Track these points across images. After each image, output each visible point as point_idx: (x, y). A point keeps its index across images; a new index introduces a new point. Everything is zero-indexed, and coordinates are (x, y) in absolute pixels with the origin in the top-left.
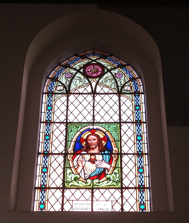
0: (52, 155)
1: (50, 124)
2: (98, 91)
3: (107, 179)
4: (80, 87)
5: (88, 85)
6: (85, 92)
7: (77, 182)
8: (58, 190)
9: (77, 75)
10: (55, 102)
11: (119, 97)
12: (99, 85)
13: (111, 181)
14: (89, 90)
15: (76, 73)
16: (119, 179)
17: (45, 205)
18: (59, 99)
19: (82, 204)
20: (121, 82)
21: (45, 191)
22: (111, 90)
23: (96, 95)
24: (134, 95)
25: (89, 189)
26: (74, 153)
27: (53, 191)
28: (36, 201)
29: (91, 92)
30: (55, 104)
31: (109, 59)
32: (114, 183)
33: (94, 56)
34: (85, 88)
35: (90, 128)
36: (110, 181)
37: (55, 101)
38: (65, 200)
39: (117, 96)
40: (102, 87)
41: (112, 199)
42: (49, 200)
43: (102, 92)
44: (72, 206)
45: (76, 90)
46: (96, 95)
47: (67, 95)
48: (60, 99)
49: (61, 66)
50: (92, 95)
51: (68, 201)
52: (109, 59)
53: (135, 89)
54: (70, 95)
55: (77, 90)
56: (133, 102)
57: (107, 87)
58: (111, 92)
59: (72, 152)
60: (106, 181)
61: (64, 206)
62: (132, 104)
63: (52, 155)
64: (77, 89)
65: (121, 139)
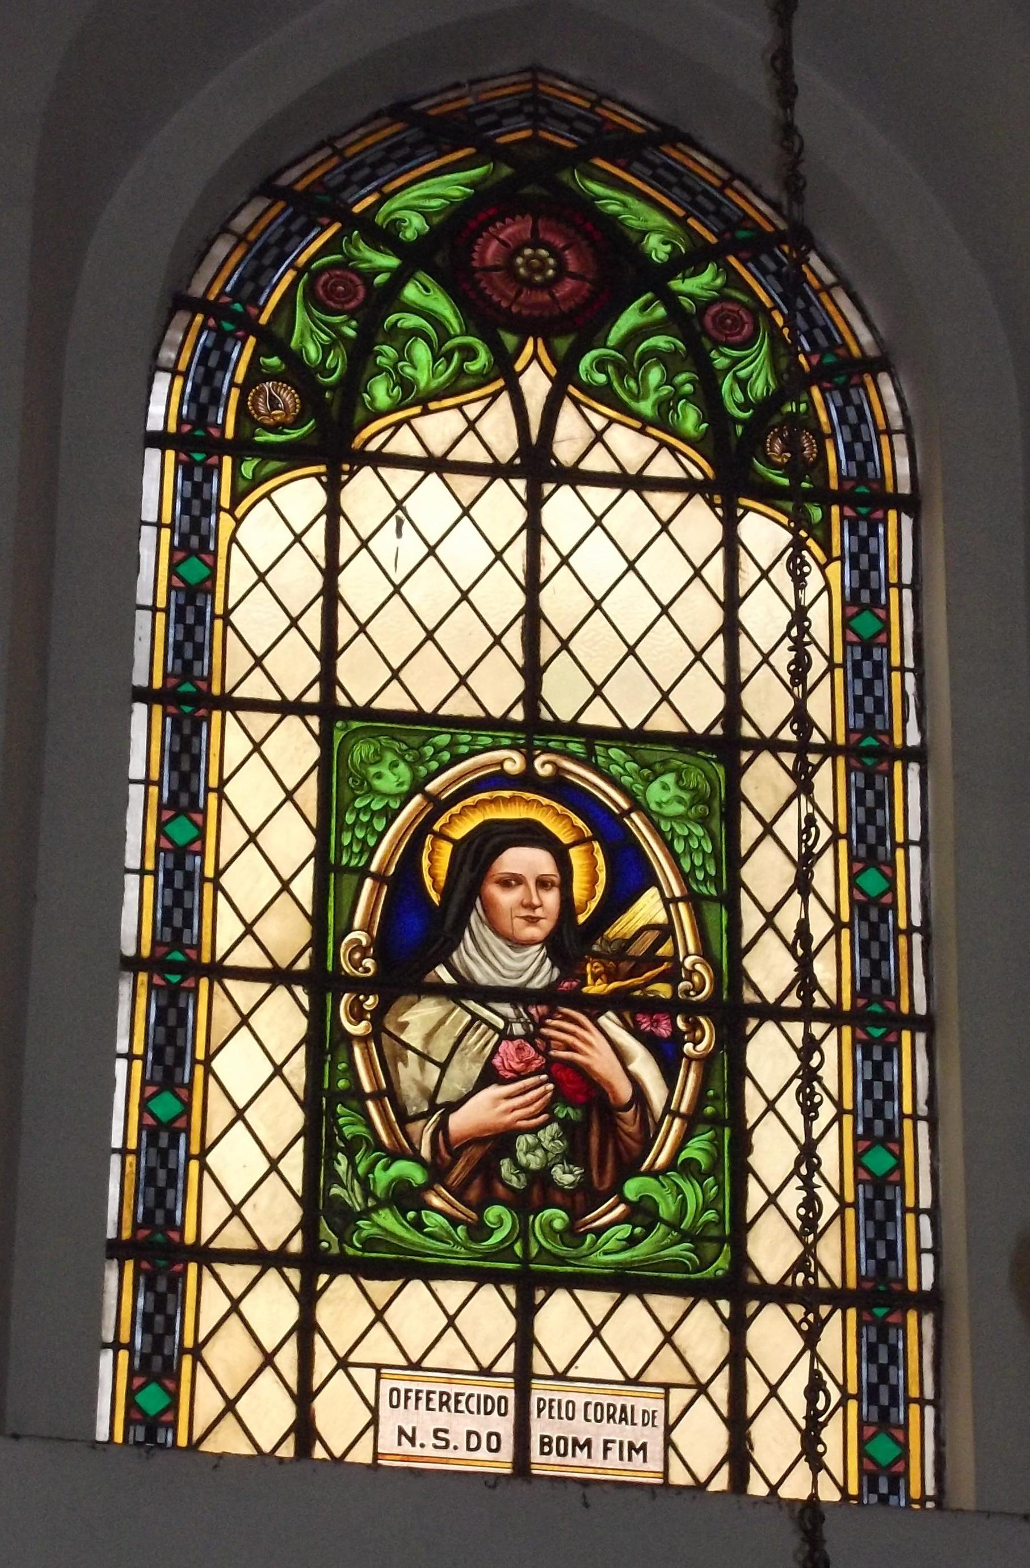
0: (229, 715)
1: (227, 299)
2: (565, 451)
3: (625, 948)
4: (433, 406)
5: (495, 396)
6: (470, 451)
7: (411, 1215)
8: (293, 722)
9: (411, 292)
10: (239, 522)
11: (730, 523)
12: (577, 403)
13: (660, 1230)
14: (506, 446)
15: (399, 278)
16: (721, 1214)
17: (211, 563)
18: (266, 502)
19: (445, 1398)
20: (743, 384)
21: (228, 295)
22: (673, 450)
23: (553, 486)
24: (859, 1316)
25: (497, 1278)
26: (376, 972)
27: (259, 722)
28: (142, 787)
29: (518, 461)
30: (233, 539)
31: (652, 166)
32: (681, 1250)
33: (535, 128)
34: (472, 410)
35: (508, 766)
36: (649, 1229)
37: (239, 512)
38: (323, 1363)
39: (712, 506)
40: (599, 422)
41: (666, 1367)
42: (234, 618)
43: (597, 462)
44: (374, 1410)
45: (398, 425)
46: (553, 486)
47: (322, 468)
48: (274, 496)
49: (281, 205)
50: (520, 485)
51: (340, 1373)
52: (652, 166)
53: (860, 409)
54: (352, 474)
55: (405, 428)
56: (834, 570)
57: (637, 424)
58: (665, 467)
59: (367, 970)
60: (624, 1231)
61: (342, 578)
62: (827, 587)
63: (229, 715)
64: (407, 421)
65: (737, 884)
